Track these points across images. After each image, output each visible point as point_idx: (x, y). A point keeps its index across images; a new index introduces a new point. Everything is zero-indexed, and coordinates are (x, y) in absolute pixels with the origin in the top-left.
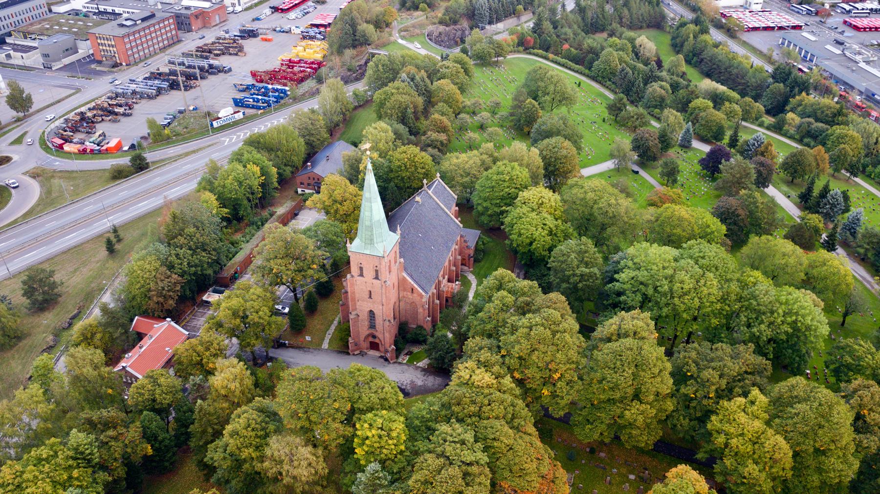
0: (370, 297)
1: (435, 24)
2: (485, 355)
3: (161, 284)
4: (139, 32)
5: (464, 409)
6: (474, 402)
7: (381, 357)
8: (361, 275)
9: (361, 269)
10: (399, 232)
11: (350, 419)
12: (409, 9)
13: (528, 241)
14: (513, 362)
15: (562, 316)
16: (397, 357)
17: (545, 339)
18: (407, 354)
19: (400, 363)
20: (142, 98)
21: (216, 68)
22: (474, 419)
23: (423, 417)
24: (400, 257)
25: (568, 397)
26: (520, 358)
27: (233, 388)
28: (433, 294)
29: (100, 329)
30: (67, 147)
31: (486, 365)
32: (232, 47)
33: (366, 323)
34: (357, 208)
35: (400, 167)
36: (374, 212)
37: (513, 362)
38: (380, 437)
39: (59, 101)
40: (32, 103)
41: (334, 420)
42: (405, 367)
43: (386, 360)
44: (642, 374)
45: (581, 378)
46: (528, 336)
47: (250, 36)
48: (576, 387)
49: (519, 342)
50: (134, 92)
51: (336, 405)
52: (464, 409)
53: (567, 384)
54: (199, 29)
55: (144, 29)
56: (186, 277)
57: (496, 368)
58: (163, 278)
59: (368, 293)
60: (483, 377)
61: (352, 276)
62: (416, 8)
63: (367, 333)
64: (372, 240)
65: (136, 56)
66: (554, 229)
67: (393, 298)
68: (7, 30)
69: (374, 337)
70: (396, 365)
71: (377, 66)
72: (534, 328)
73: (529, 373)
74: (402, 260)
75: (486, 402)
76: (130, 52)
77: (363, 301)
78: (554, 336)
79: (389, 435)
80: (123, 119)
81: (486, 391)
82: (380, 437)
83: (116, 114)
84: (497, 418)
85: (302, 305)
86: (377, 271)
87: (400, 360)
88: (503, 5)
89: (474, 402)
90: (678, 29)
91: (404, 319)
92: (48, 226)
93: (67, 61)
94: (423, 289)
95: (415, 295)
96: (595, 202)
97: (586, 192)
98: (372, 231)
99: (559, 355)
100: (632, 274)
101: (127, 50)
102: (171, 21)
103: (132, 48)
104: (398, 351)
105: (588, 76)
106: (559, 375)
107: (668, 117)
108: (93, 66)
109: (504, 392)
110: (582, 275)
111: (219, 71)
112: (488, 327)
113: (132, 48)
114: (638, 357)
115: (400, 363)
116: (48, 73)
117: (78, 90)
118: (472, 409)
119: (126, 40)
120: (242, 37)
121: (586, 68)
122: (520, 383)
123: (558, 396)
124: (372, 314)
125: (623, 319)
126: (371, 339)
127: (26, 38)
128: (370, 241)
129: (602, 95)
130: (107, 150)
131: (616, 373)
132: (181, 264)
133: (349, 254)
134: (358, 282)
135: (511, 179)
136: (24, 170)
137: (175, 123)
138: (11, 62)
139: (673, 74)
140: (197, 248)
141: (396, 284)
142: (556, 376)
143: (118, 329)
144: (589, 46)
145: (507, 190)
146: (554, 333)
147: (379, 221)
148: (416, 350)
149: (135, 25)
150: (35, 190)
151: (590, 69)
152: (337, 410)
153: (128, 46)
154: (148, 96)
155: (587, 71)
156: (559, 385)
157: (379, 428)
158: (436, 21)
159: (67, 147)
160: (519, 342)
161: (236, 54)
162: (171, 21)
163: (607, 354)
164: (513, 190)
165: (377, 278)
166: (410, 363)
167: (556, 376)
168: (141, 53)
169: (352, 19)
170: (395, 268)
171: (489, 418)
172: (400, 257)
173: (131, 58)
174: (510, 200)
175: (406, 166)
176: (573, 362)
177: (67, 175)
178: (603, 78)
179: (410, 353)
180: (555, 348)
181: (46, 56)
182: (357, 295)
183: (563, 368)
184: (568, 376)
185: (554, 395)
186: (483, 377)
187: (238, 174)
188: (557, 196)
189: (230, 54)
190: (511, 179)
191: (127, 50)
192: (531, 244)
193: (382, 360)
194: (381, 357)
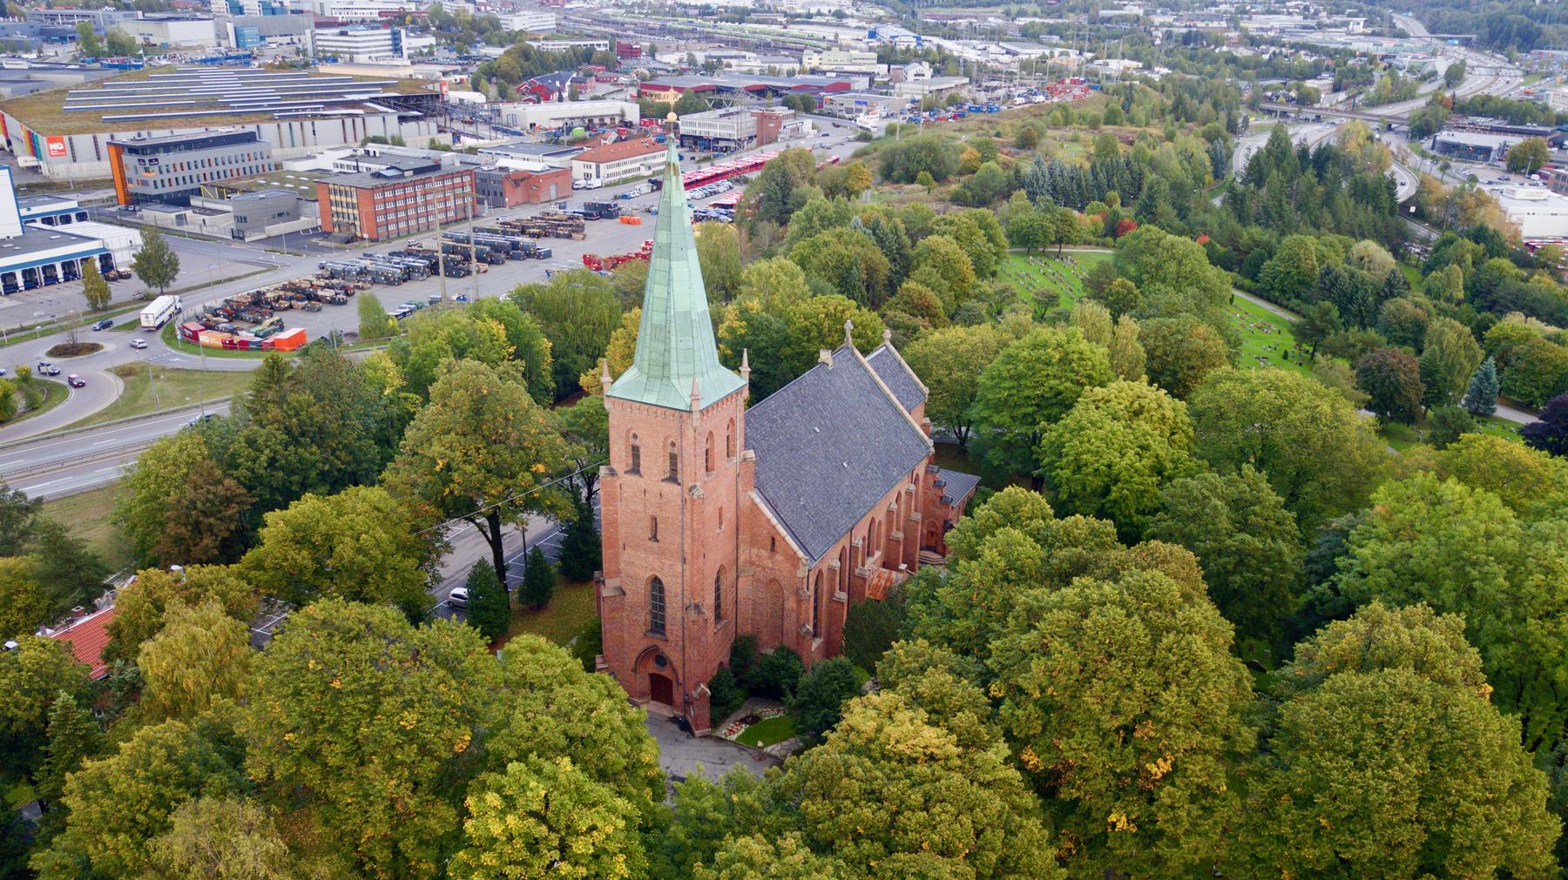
0: (654, 538)
1: (943, 200)
2: (936, 680)
3: (190, 494)
4: (404, 186)
5: (838, 810)
6: (874, 796)
7: (674, 720)
8: (635, 470)
9: (635, 450)
10: (745, 368)
11: (454, 781)
12: (898, 182)
13: (1098, 482)
14: (1026, 716)
15: (1187, 598)
16: (715, 723)
17: (1125, 645)
18: (743, 721)
19: (719, 740)
20: (374, 282)
21: (523, 248)
22: (866, 846)
23: (701, 818)
24: (746, 447)
25: (1194, 841)
26: (1047, 707)
27: (189, 683)
28: (831, 570)
29: (31, 585)
30: (204, 338)
31: (938, 712)
32: (569, 228)
33: (643, 617)
34: (643, 288)
35: (806, 331)
36: (677, 286)
37: (1026, 716)
38: (533, 845)
39: (231, 280)
40: (176, 271)
41: (391, 766)
42: (732, 750)
43: (685, 726)
44: (1454, 783)
45: (1238, 784)
46: (1074, 634)
47: (602, 216)
48: (1222, 813)
49: (1045, 651)
50: (363, 272)
51: (410, 719)
52: (838, 810)
53: (1193, 799)
54: (517, 204)
55: (414, 184)
56: (258, 490)
57: (965, 718)
58: (200, 481)
59: (647, 524)
60: (914, 732)
61: (613, 473)
62: (911, 179)
63: (643, 645)
64: (666, 365)
65: (392, 227)
66: (1169, 465)
67: (718, 551)
68: (196, 185)
69: (662, 660)
70: (707, 742)
71: (810, 219)
72: (1094, 612)
73: (1071, 748)
74: (751, 454)
75: (916, 797)
76: (381, 219)
77: (637, 547)
78: (1156, 639)
79: (563, 848)
80: (327, 309)
81: (921, 769)
82: (533, 845)
83: (318, 299)
84: (946, 852)
85: (515, 577)
86: (673, 458)
87: (722, 732)
88: (1079, 187)
89: (874, 796)
90: (1436, 250)
91: (747, 629)
92: (98, 445)
93: (275, 229)
94: (803, 546)
95: (779, 557)
96: (1280, 412)
97: (1253, 392)
98: (666, 341)
99: (1169, 697)
100: (1388, 550)
101: (376, 214)
102: (467, 179)
103: (386, 212)
104: (720, 707)
105: (1249, 291)
106: (1165, 767)
107: (1442, 333)
108: (314, 240)
109: (986, 785)
110: (1239, 552)
111: (529, 256)
112: (961, 625)
113: (386, 212)
114: (1440, 728)
115: (719, 740)
116: (237, 245)
117: (272, 268)
118: (867, 812)
119: (378, 197)
120: (587, 216)
121: (1246, 275)
122: (1045, 785)
123: (1161, 833)
124: (656, 582)
125: (1378, 623)
126: (653, 667)
127: (221, 197)
128: (662, 372)
129: (1278, 321)
130: (273, 344)
131: (1361, 767)
132: (254, 460)
133: (608, 405)
134: (627, 492)
135: (1065, 360)
136: (109, 366)
137: (417, 315)
138: (185, 228)
139: (1438, 297)
140: (303, 434)
141: (729, 515)
142: (1159, 768)
143: (73, 589)
144: (1252, 238)
145: (1053, 382)
146: (1156, 634)
147: (687, 314)
148: (770, 713)
149: (402, 176)
150: (116, 388)
151: (1254, 277)
152: (410, 736)
153: (380, 208)
154: (387, 278)
155: (1247, 282)
156: (1165, 794)
157: (532, 814)
158: (948, 197)
159: (204, 338)
160: (1045, 651)
161: (569, 237)
162: (467, 179)
163: (1331, 707)
164: (1068, 384)
165: (673, 479)
166: (742, 744)
167: (1159, 768)
168: (402, 225)
169: (784, 175)
170: (728, 469)
171: (915, 848)
172: (746, 447)
173: (382, 230)
174: (1059, 404)
175: (820, 332)
176: (1214, 730)
177: (184, 375)
178: (1283, 292)
179: (753, 720)
180: (1154, 676)
181: (241, 219)
182: (622, 531)
183: (1182, 739)
184: (1197, 770)
185: (1148, 834)
186: (914, 732)
187: (457, 332)
188: (1181, 405)
189: (558, 236)
190: (1065, 360)
191: (376, 214)
192: (1106, 491)
193: (675, 727)
194: (674, 720)
